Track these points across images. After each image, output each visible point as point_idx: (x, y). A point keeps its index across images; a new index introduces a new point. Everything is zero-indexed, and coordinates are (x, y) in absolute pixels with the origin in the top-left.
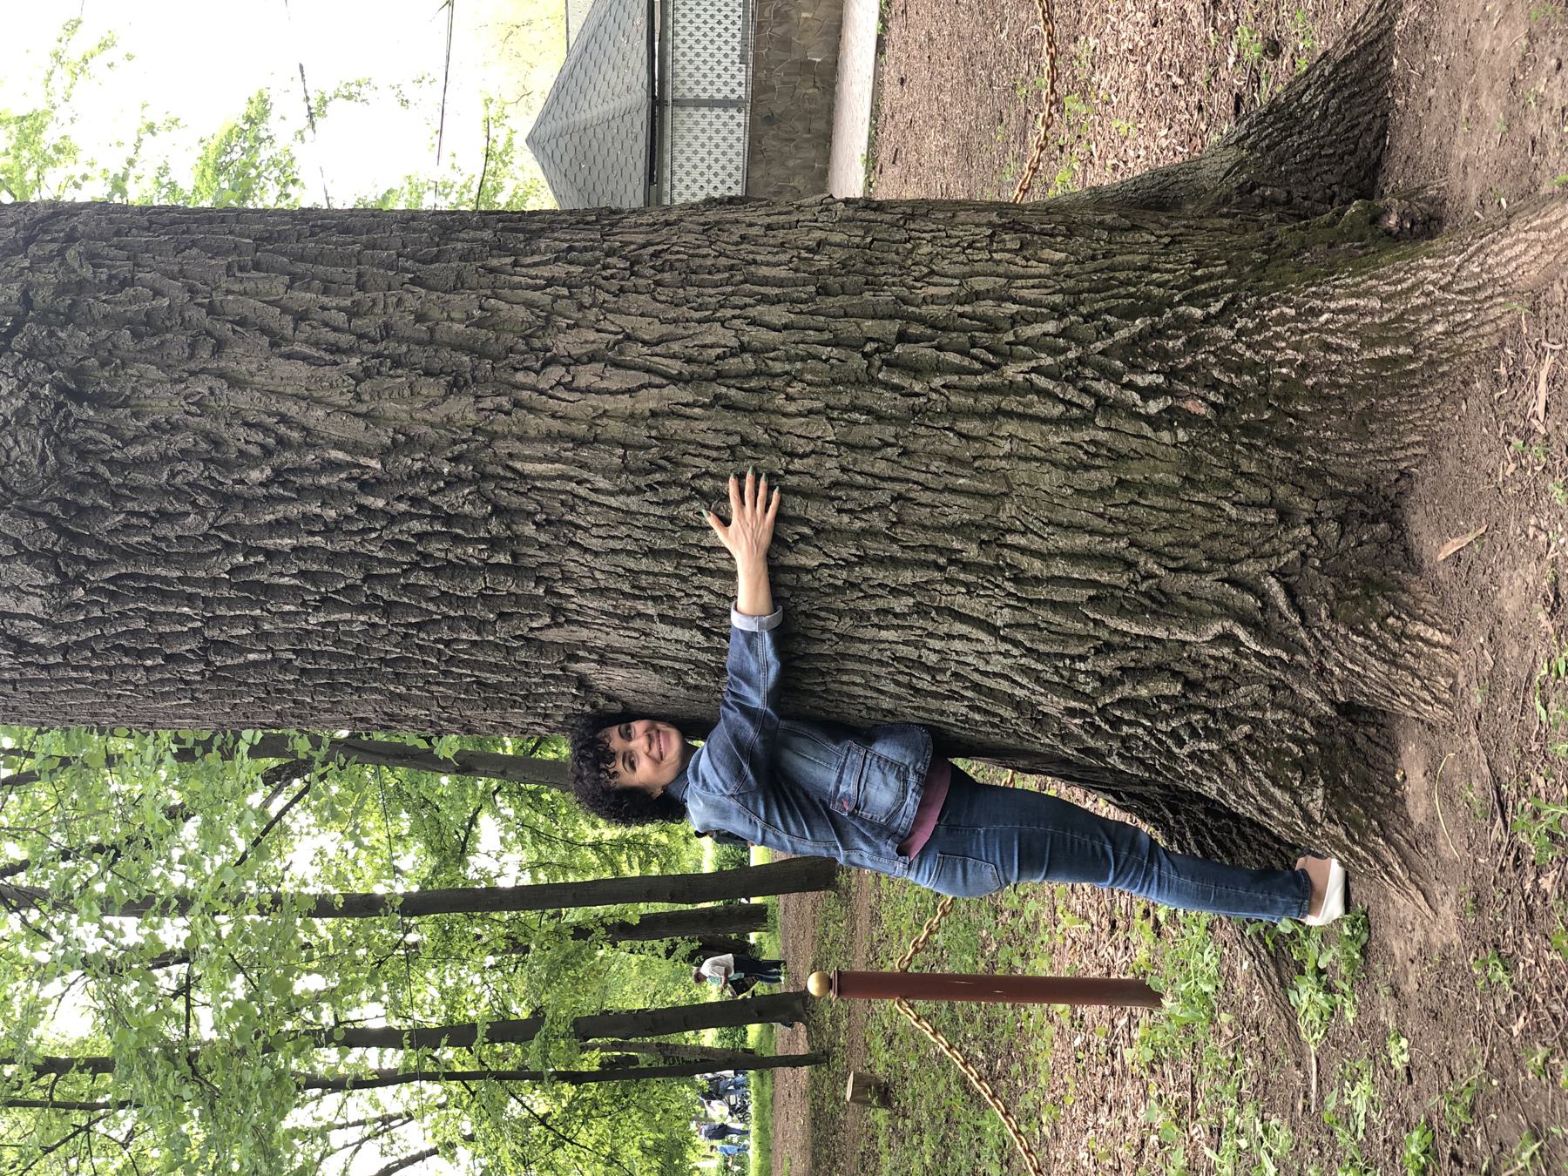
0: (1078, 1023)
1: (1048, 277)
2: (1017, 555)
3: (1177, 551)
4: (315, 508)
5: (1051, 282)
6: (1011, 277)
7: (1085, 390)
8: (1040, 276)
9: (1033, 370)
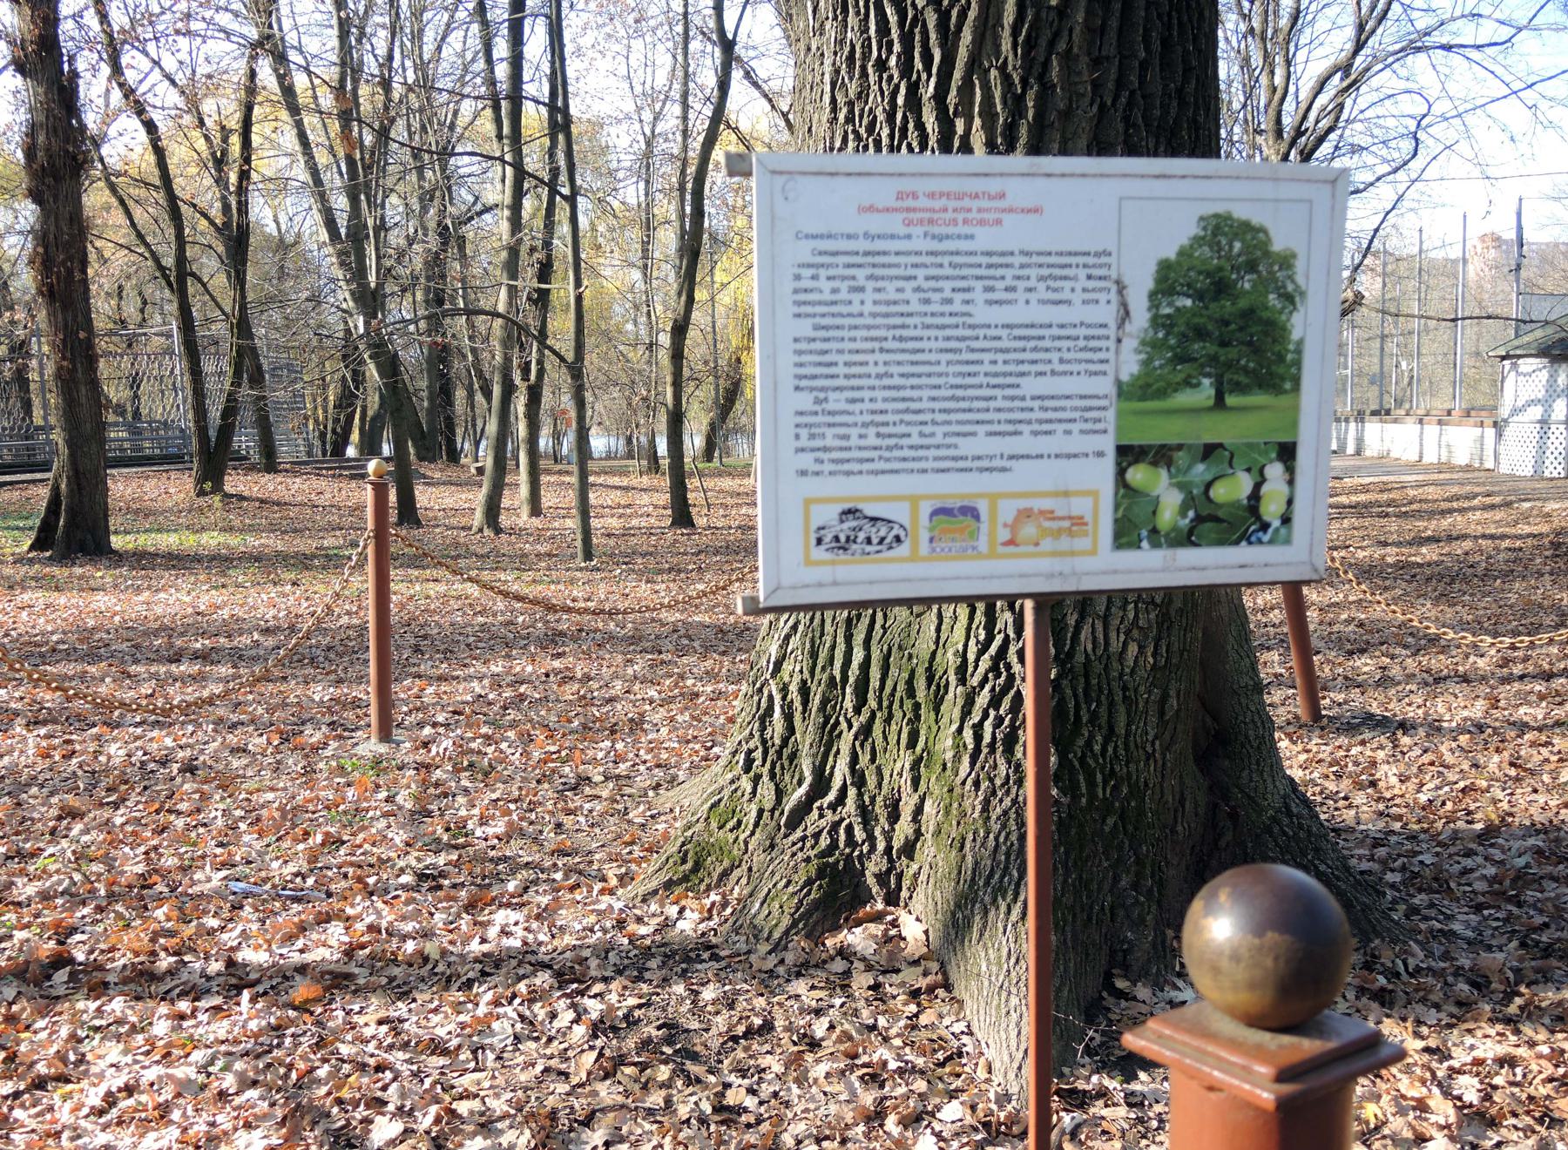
0: (578, 52)
1: (1106, 649)
2: (867, 621)
3: (868, 748)
4: (897, 48)
5: (1100, 652)
6: (1106, 620)
7: (985, 680)
8: (1107, 643)
9: (1007, 636)
